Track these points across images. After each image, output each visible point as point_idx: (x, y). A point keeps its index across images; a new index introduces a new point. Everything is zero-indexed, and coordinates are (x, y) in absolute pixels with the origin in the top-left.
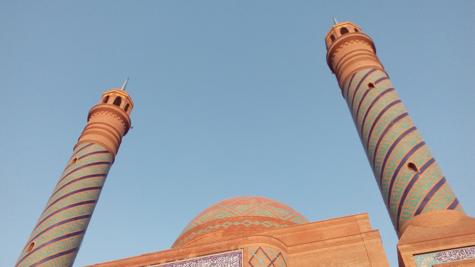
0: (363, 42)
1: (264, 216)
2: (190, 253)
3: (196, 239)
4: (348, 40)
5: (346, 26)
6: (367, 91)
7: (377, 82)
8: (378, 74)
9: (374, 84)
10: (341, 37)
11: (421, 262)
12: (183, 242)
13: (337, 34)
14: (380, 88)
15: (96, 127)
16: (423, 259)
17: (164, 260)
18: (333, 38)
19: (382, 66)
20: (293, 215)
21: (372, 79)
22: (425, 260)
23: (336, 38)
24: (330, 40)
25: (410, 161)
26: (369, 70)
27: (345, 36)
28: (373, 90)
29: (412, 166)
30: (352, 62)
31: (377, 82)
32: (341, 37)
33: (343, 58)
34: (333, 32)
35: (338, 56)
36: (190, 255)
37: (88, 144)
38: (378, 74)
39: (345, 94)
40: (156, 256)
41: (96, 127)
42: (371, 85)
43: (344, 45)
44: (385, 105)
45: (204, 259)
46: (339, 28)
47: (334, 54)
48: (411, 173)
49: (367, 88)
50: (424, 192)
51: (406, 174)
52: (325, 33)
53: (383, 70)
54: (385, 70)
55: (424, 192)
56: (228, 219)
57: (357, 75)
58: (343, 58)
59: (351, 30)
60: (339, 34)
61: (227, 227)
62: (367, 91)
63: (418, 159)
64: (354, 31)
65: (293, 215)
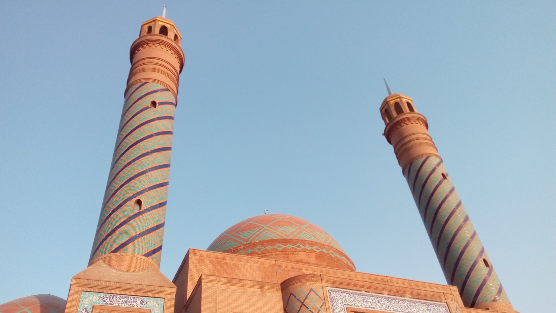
0: (177, 56)
1: (268, 239)
2: (406, 293)
3: (287, 253)
4: (161, 42)
5: (168, 26)
6: (147, 108)
7: (162, 103)
8: (168, 97)
9: (157, 105)
10: (156, 35)
11: (85, 298)
12: (266, 250)
13: (156, 29)
14: (160, 111)
15: (152, 63)
16: (90, 296)
17: (386, 292)
18: (150, 29)
19: (429, 136)
20: (300, 230)
21: (158, 98)
22: (91, 298)
23: (152, 33)
24: (147, 30)
25: (141, 197)
26: (160, 87)
27: (163, 38)
28: (153, 109)
29: (139, 202)
30: (151, 70)
31: (162, 103)
32: (156, 35)
33: (151, 58)
34: (153, 23)
35: (143, 53)
36: (407, 295)
37: (408, 167)
38: (168, 97)
39: (127, 96)
40: (128, 286)
41: (152, 63)
42: (154, 104)
43: (159, 47)
44: (154, 131)
45: (420, 302)
46: (161, 24)
47: (141, 48)
48: (137, 209)
49: (149, 104)
50: (134, 232)
51: (131, 208)
52: (147, 18)
53: (176, 96)
54: (178, 97)
55: (134, 232)
56: (316, 244)
57: (148, 85)
58: (151, 58)
59: (171, 35)
60: (157, 30)
61: (318, 251)
62: (147, 108)
63: (148, 200)
64: (172, 37)
65: (300, 230)
